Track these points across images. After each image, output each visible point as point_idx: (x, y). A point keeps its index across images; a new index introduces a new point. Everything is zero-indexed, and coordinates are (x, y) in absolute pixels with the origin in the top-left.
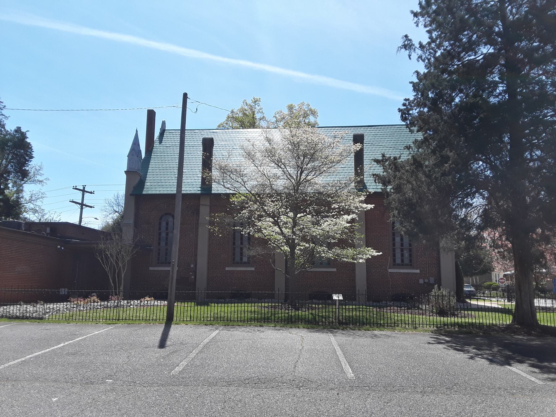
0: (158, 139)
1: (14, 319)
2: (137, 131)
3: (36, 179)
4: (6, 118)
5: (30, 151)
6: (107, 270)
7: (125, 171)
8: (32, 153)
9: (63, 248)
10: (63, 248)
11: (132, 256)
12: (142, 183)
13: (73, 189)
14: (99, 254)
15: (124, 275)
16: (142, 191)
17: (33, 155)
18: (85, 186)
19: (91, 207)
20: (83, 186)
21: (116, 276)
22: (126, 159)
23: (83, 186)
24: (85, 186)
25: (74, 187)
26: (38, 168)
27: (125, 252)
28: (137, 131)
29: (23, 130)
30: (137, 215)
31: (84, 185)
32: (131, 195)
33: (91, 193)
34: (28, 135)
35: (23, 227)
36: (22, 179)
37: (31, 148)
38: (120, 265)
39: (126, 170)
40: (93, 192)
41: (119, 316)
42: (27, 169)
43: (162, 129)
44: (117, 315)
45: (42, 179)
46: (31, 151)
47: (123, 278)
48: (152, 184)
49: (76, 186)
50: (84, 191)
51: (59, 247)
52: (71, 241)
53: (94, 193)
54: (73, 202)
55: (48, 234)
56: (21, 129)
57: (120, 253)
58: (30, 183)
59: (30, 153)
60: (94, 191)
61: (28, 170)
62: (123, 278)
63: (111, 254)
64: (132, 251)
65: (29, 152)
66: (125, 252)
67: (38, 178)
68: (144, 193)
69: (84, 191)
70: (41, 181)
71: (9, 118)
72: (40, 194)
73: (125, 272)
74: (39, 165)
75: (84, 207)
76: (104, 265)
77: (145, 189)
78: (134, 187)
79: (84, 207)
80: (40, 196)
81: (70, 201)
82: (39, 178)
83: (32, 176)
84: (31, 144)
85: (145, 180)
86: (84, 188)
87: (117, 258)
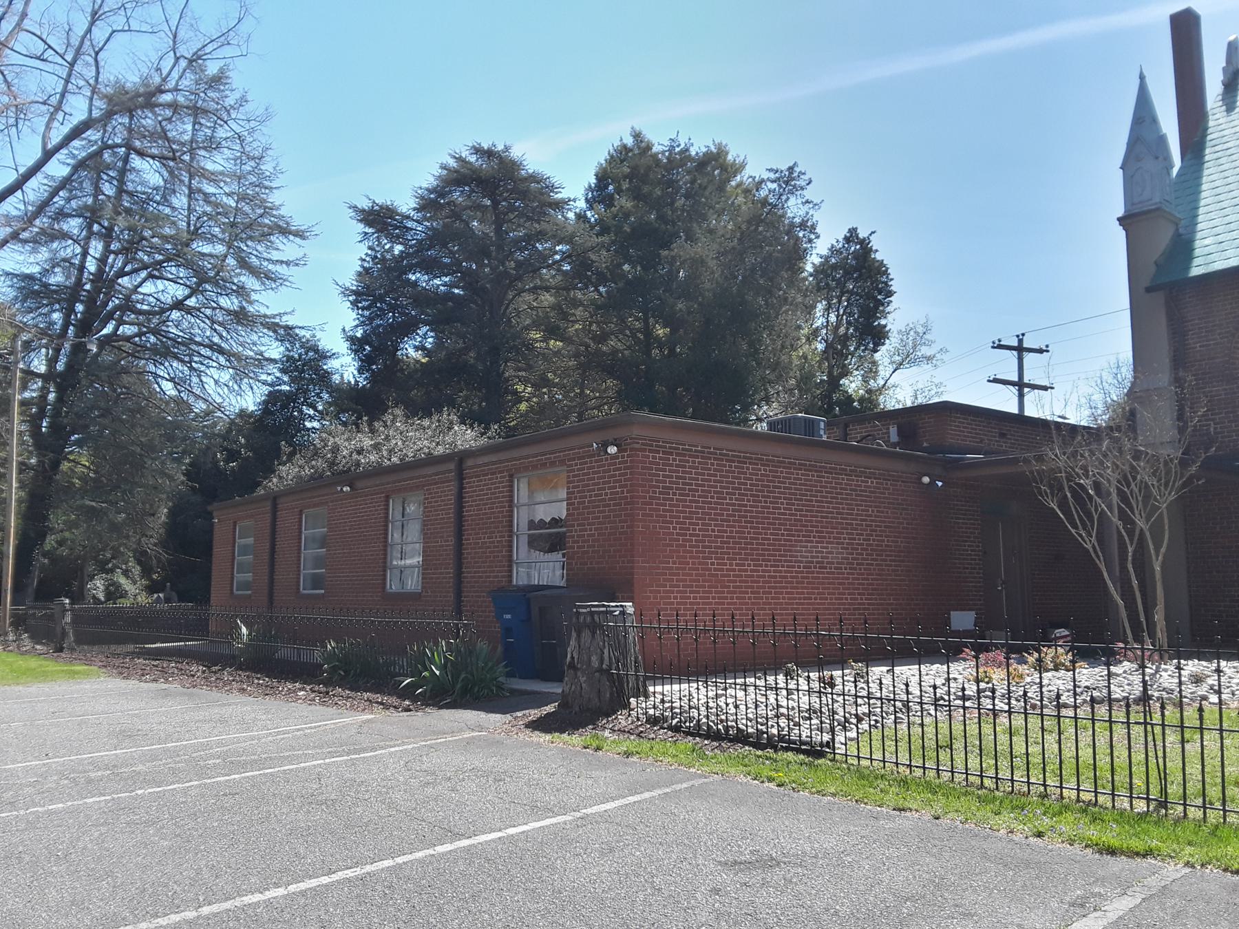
0: (1221, 103)
1: (730, 741)
2: (1142, 78)
3: (920, 354)
4: (817, 207)
5: (884, 279)
6: (1088, 546)
7: (1119, 219)
8: (890, 283)
9: (940, 484)
10: (940, 484)
11: (1184, 485)
12: (1183, 247)
13: (993, 347)
14: (1051, 487)
15: (1164, 566)
16: (1188, 267)
17: (892, 288)
18: (1023, 335)
19: (1045, 388)
20: (1018, 336)
21: (1130, 566)
22: (1118, 177)
23: (1018, 336)
24: (1023, 335)
25: (994, 343)
26: (920, 330)
27: (1154, 474)
28: (1142, 78)
29: (862, 234)
30: (1179, 360)
31: (1019, 333)
32: (1149, 290)
33: (1040, 351)
34: (875, 243)
35: (822, 432)
36: (874, 347)
37: (886, 273)
38: (1140, 523)
39: (1121, 212)
40: (1044, 348)
41: (1164, 777)
42: (883, 322)
43: (1231, 69)
44: (1154, 774)
45: (933, 353)
46: (887, 277)
47: (1158, 576)
48: (1220, 238)
49: (1000, 341)
50: (1020, 349)
51: (926, 480)
52: (963, 459)
53: (1048, 351)
54: (996, 381)
55: (894, 445)
56: (858, 231)
57: (1134, 479)
58: (908, 366)
59: (886, 283)
60: (1047, 346)
61: (885, 326)
62: (1158, 576)
63: (1097, 485)
64: (1184, 463)
65: (883, 283)
66: (1154, 474)
67: (923, 352)
68: (1195, 271)
69: (1020, 349)
70: (929, 359)
71: (822, 205)
72: (934, 387)
73: (1163, 550)
74: (922, 323)
75: (1026, 390)
76: (1076, 527)
77: (1196, 262)
78: (1156, 263)
79: (1026, 390)
80: (933, 392)
81: (989, 381)
82: (925, 350)
83: (911, 351)
84: (885, 262)
85: (1194, 232)
86: (1021, 341)
87: (1121, 493)
